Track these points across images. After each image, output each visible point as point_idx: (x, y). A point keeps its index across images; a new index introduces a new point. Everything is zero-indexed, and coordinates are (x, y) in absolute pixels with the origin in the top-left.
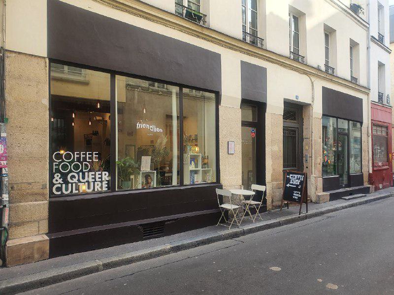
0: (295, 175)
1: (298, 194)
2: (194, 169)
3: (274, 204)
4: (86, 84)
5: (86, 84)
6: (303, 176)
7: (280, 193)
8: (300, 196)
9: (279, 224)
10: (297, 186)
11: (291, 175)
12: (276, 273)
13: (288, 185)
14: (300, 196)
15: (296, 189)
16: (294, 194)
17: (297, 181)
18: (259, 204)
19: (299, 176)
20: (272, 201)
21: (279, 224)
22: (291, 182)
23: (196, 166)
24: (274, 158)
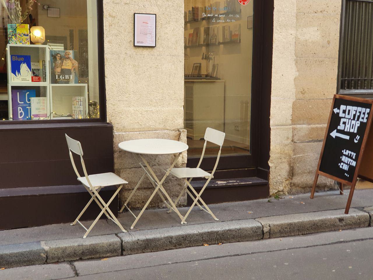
0: (349, 107)
1: (350, 157)
2: (29, 83)
3: (297, 180)
4: (348, 124)
5: (348, 124)
6: (368, 110)
7: (313, 154)
8: (354, 164)
9: (260, 234)
10: (352, 135)
11: (343, 107)
12: (350, 266)
13: (334, 134)
14: (354, 164)
15: (349, 145)
16: (344, 158)
17: (353, 122)
18: (204, 179)
19: (359, 109)
20: (292, 173)
21: (260, 234)
22: (341, 127)
23: (36, 75)
24: (303, 57)
